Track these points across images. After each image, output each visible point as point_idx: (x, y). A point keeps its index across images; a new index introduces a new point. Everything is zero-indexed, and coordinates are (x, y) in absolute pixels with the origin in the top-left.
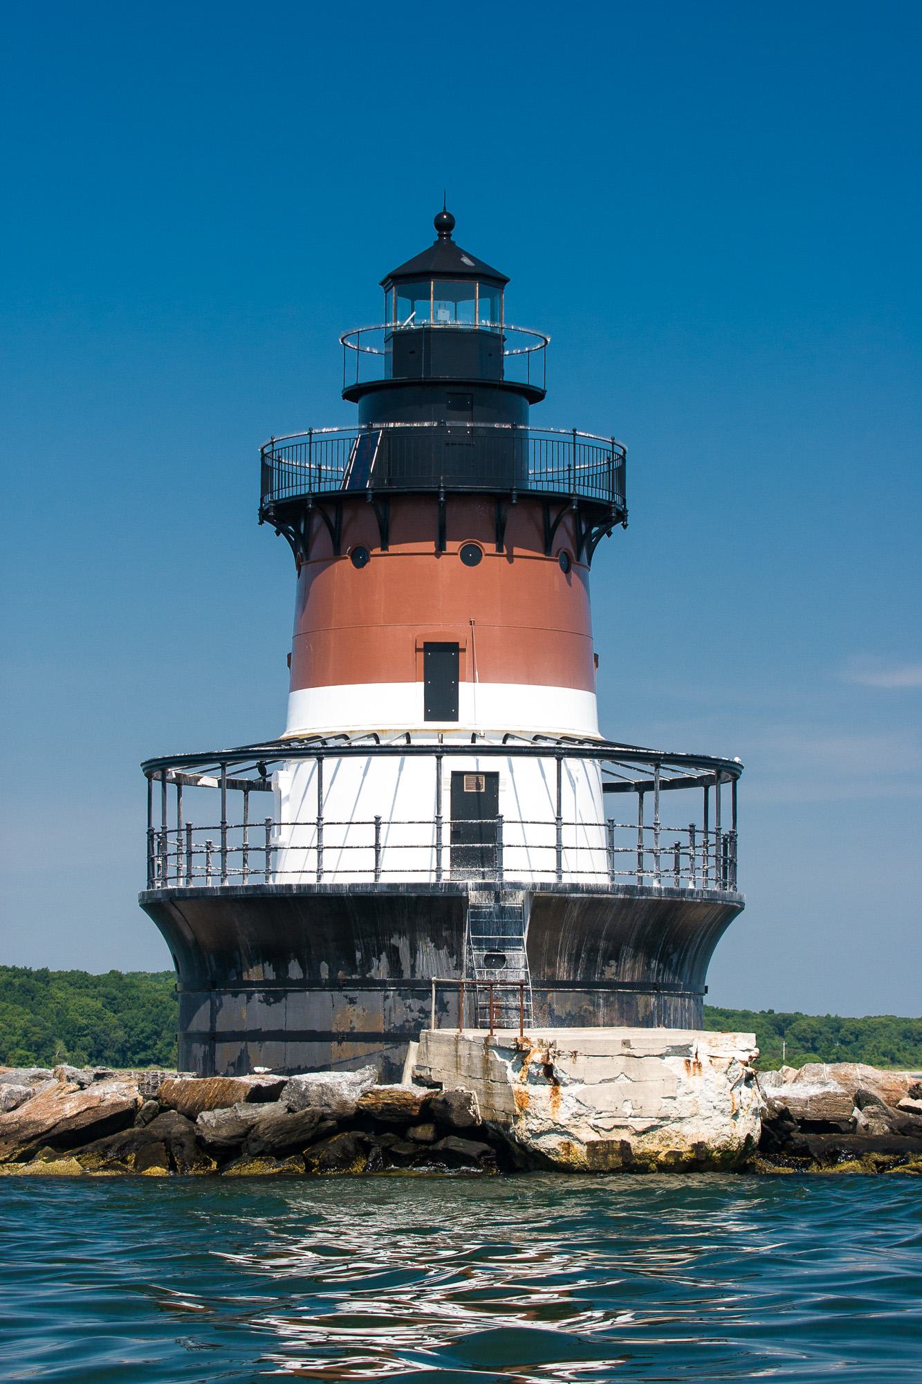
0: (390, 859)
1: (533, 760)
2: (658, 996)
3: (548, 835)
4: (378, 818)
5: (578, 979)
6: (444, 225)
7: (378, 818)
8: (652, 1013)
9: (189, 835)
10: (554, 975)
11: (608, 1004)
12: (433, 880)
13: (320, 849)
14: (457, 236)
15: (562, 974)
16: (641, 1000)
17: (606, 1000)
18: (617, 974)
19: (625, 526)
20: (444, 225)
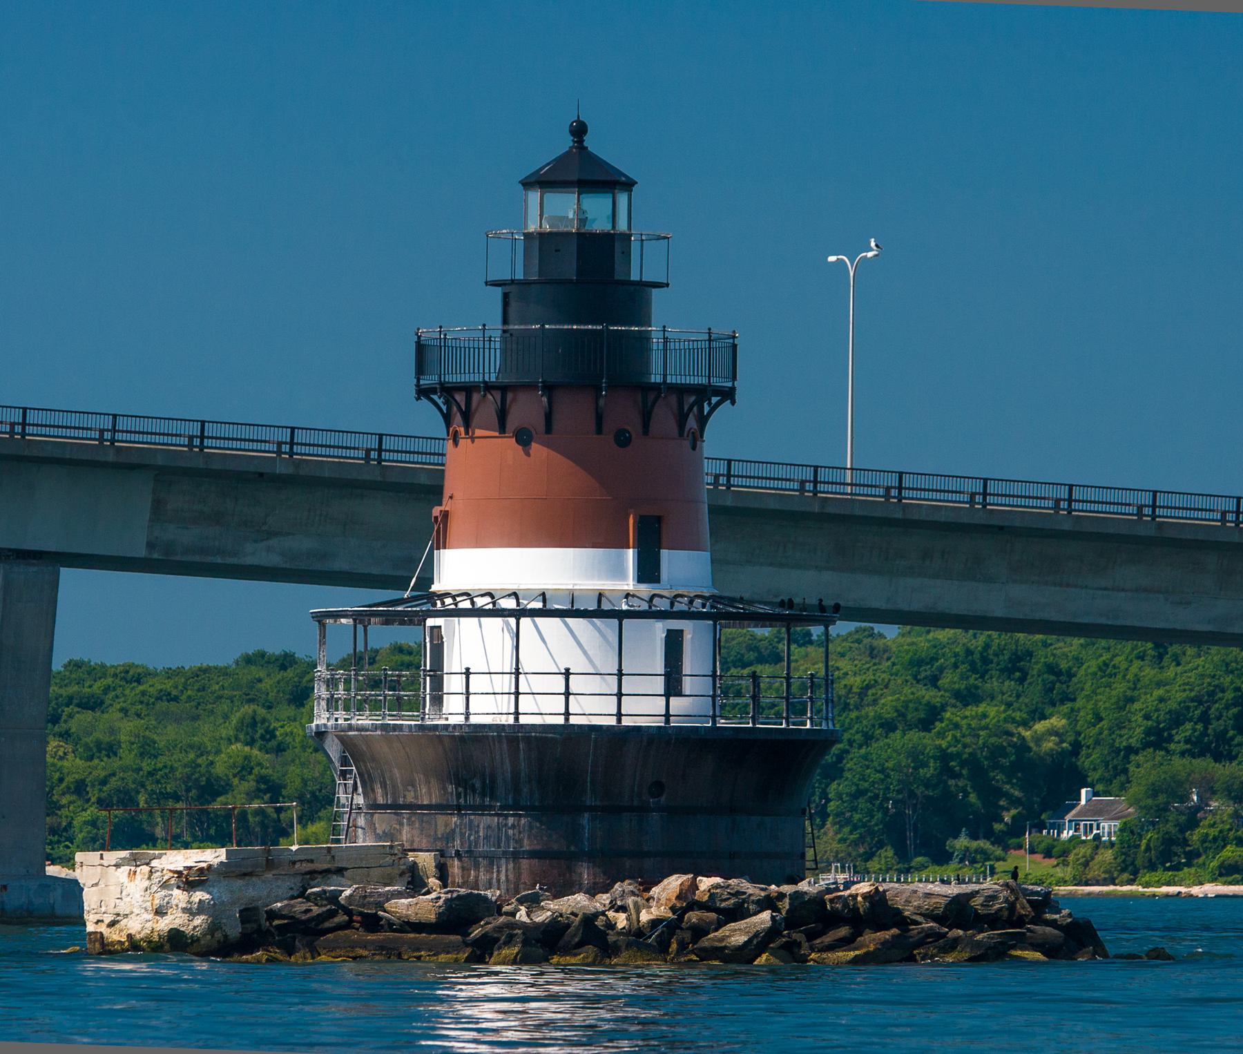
0: (628, 705)
1: (474, 621)
2: (460, 815)
3: (507, 683)
4: (468, 669)
5: (434, 802)
6: (579, 131)
7: (468, 669)
8: (453, 831)
9: (714, 671)
10: (375, 799)
11: (411, 823)
12: (614, 723)
13: (620, 695)
14: (588, 141)
15: (380, 800)
16: (441, 819)
17: (409, 819)
18: (416, 797)
19: (733, 403)
20: (579, 131)
